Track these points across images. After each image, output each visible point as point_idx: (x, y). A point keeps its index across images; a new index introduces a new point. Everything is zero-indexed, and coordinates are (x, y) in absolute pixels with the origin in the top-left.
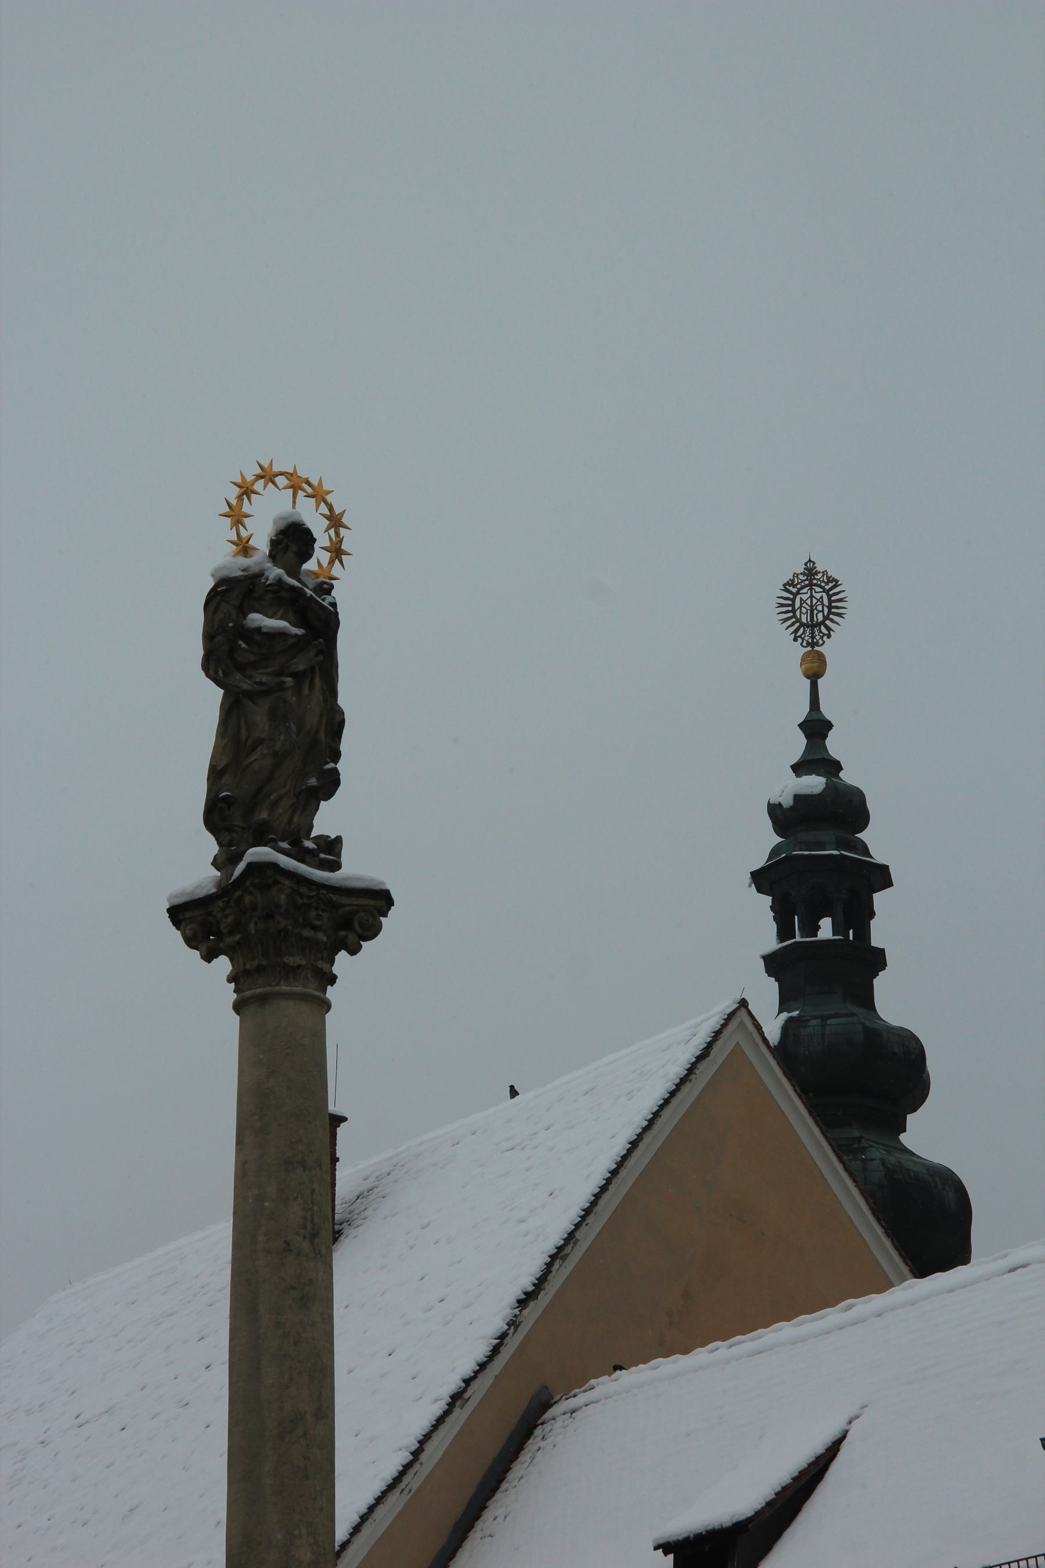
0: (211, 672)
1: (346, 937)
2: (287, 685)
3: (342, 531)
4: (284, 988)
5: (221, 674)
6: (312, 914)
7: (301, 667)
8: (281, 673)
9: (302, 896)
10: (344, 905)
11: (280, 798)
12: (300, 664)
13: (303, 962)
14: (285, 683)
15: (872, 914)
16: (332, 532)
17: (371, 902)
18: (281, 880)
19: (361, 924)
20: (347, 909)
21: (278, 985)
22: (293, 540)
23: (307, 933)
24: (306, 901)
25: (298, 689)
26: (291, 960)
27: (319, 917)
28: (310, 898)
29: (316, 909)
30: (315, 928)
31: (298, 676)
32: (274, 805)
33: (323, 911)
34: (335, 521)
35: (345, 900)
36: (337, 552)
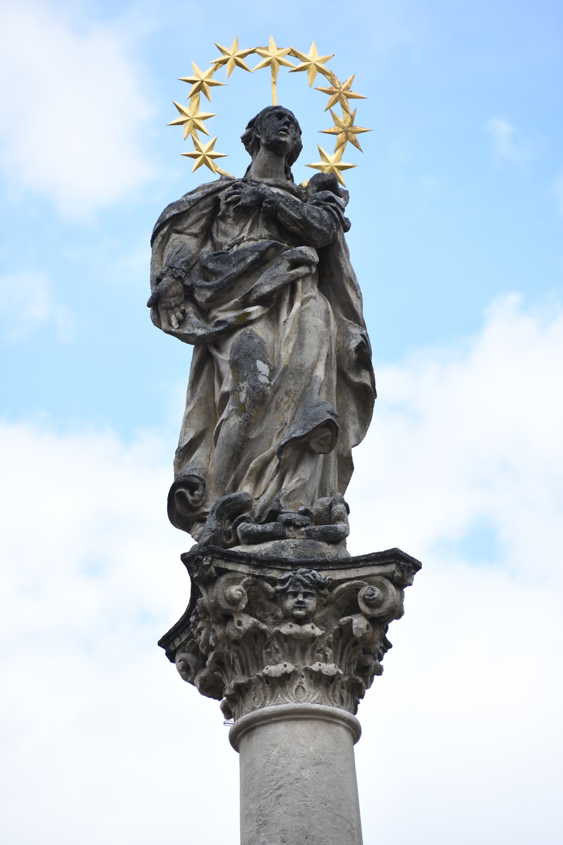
0: (164, 325)
1: (350, 622)
2: (254, 316)
3: (351, 104)
4: (270, 708)
5: (174, 322)
6: (290, 603)
7: (267, 289)
8: (246, 303)
9: (273, 582)
10: (341, 582)
11: (266, 463)
12: (265, 284)
13: (290, 668)
14: (249, 314)
15: (376, 396)
16: (337, 108)
17: (377, 570)
18: (230, 567)
19: (367, 602)
20: (344, 585)
21: (263, 705)
22: (272, 135)
23: (285, 629)
24: (279, 587)
25: (273, 316)
26: (273, 670)
27: (300, 605)
28: (283, 582)
29: (295, 595)
30: (300, 621)
31: (263, 301)
32: (259, 475)
33: (305, 595)
34: (340, 96)
35: (339, 575)
36: (348, 135)
